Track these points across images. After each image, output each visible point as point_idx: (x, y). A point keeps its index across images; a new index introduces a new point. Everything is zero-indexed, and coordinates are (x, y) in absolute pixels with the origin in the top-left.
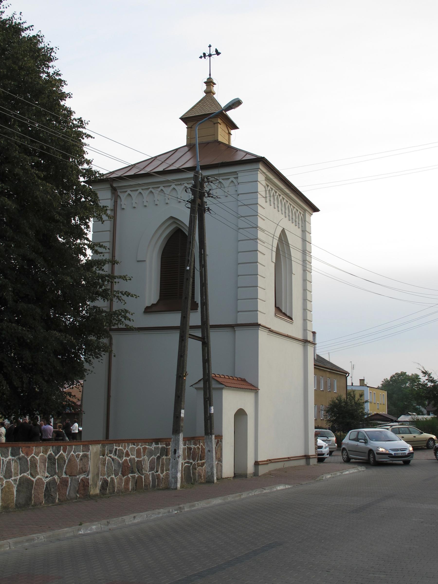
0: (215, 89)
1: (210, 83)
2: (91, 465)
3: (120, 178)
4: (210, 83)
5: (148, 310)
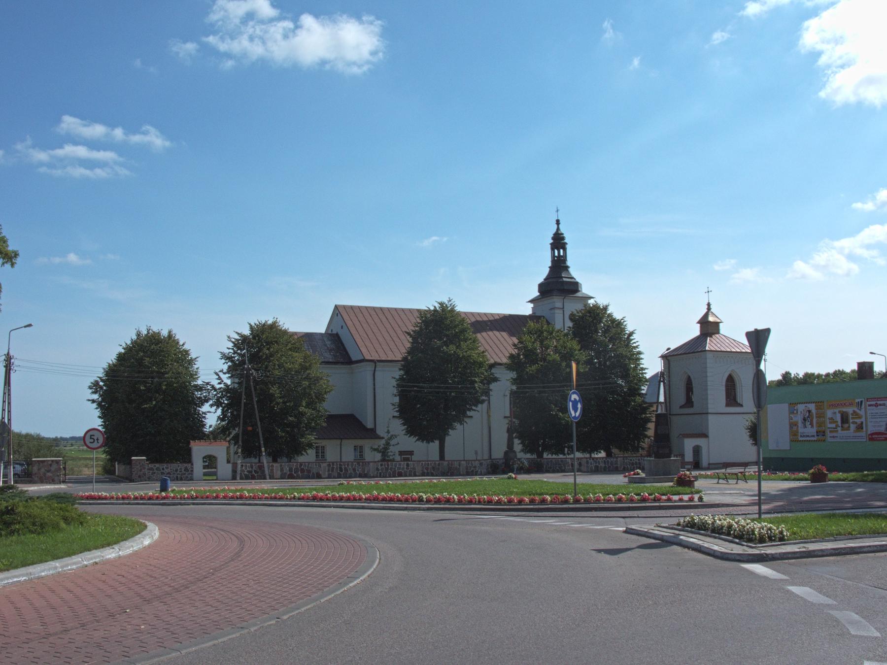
0: (711, 307)
1: (709, 305)
2: (619, 463)
3: (669, 356)
4: (709, 305)
5: (681, 407)
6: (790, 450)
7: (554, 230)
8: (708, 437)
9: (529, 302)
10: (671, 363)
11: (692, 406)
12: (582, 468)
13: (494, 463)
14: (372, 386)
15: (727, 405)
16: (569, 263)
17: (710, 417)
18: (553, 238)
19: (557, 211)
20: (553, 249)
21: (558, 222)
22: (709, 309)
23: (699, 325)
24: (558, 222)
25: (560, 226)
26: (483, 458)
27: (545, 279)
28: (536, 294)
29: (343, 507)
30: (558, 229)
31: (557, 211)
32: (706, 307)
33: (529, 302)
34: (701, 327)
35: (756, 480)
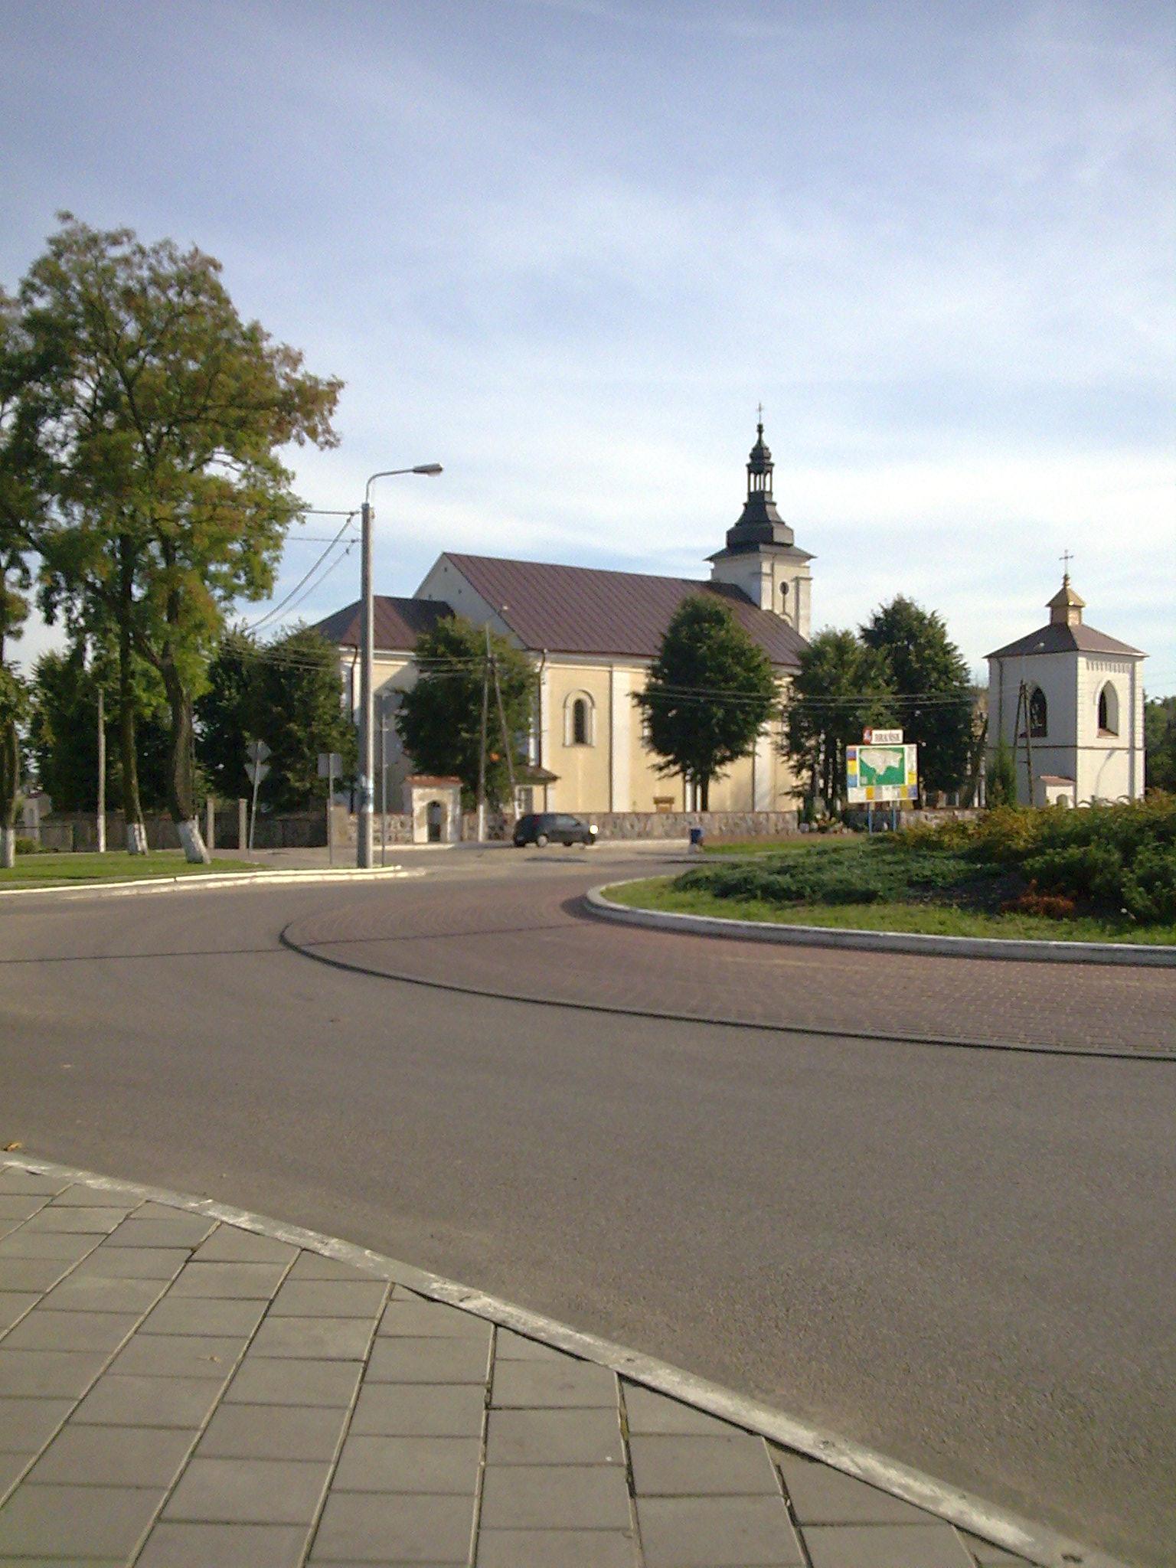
0: (1069, 582)
1: (1066, 578)
4: (1066, 578)
6: (1057, 805)
7: (754, 443)
8: (1075, 781)
9: (708, 559)
10: (1005, 668)
11: (1045, 734)
12: (764, 815)
13: (234, 660)
14: (1112, 1060)
15: (1099, 736)
16: (775, 499)
17: (1079, 752)
18: (752, 456)
19: (760, 409)
20: (750, 472)
21: (760, 429)
22: (1065, 585)
23: (1049, 609)
24: (760, 429)
25: (763, 435)
26: (636, 1435)
27: (737, 524)
28: (721, 544)
29: (330, 874)
30: (760, 441)
31: (760, 409)
32: (1062, 581)
33: (708, 559)
34: (1052, 612)
35: (634, 803)
